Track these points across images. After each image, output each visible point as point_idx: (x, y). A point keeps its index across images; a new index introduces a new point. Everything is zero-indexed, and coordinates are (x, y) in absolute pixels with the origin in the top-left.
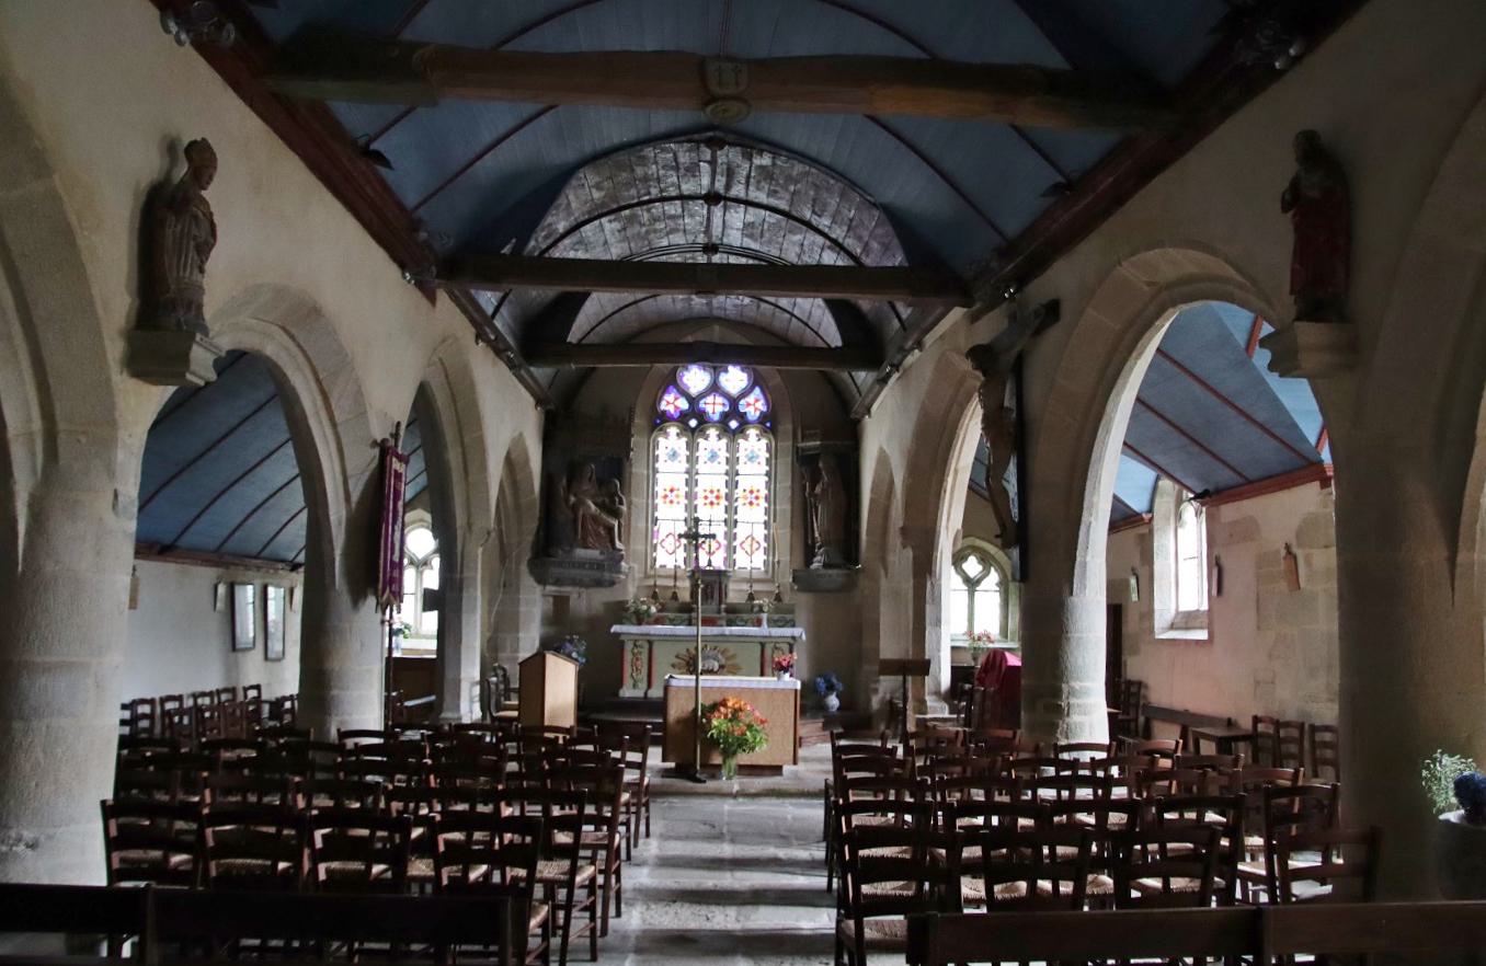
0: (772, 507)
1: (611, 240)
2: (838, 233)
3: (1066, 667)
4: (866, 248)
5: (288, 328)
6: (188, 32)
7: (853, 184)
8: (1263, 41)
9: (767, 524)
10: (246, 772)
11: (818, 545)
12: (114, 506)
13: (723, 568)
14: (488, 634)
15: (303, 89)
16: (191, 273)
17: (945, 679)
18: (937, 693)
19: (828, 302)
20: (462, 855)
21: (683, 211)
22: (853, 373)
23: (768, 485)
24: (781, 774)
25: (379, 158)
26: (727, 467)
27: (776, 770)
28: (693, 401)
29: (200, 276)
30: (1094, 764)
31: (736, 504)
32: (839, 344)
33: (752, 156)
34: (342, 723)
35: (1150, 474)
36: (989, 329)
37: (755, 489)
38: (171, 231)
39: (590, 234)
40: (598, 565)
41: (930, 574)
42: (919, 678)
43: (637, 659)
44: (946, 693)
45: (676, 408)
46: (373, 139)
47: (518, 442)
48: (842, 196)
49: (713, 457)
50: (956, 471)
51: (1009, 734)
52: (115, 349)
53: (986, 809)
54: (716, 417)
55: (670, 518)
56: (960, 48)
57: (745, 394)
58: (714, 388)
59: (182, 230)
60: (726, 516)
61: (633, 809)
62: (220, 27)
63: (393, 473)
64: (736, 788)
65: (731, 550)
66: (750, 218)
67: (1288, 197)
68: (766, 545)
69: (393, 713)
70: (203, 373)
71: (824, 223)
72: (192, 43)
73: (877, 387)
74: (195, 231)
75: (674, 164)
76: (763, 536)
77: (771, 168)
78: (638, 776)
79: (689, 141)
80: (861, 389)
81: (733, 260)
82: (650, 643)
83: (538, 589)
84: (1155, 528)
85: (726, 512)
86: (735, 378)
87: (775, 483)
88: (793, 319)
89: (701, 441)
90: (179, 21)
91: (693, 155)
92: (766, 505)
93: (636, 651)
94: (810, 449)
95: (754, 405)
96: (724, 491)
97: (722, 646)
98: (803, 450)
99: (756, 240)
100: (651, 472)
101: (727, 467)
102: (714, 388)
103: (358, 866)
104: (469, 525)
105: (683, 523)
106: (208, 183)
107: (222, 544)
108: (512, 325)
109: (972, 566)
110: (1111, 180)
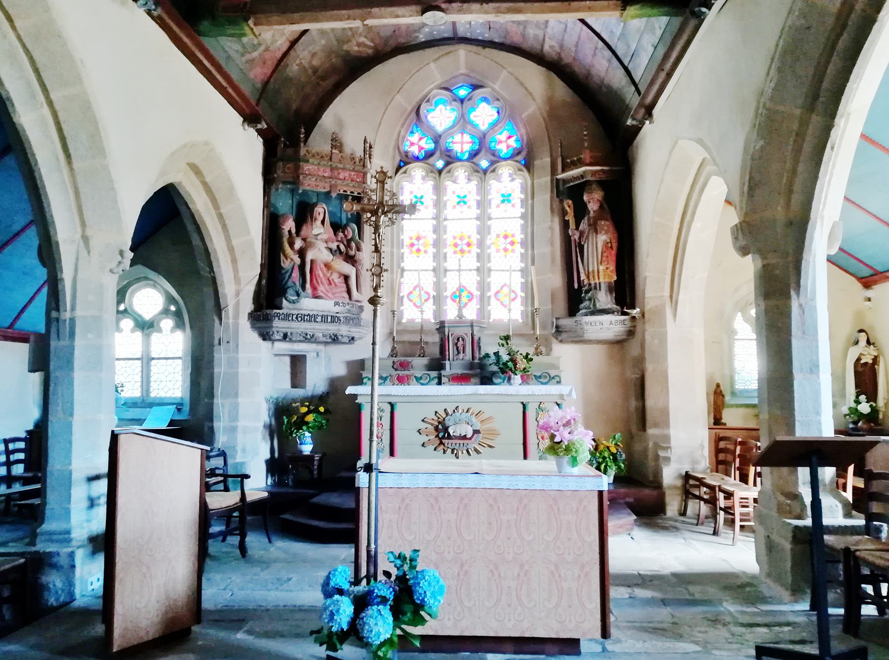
0: (530, 252)
9: (524, 272)
11: (584, 289)
14: (805, 512)
23: (524, 228)
28: (437, 139)
31: (489, 251)
37: (509, 233)
45: (421, 148)
49: (462, 201)
54: (466, 156)
60: (479, 265)
65: (484, 300)
68: (523, 295)
69: (24, 495)
76: (519, 286)
82: (392, 406)
85: (478, 261)
87: (533, 225)
89: (449, 184)
92: (523, 251)
97: (475, 408)
98: (565, 181)
105: (432, 273)
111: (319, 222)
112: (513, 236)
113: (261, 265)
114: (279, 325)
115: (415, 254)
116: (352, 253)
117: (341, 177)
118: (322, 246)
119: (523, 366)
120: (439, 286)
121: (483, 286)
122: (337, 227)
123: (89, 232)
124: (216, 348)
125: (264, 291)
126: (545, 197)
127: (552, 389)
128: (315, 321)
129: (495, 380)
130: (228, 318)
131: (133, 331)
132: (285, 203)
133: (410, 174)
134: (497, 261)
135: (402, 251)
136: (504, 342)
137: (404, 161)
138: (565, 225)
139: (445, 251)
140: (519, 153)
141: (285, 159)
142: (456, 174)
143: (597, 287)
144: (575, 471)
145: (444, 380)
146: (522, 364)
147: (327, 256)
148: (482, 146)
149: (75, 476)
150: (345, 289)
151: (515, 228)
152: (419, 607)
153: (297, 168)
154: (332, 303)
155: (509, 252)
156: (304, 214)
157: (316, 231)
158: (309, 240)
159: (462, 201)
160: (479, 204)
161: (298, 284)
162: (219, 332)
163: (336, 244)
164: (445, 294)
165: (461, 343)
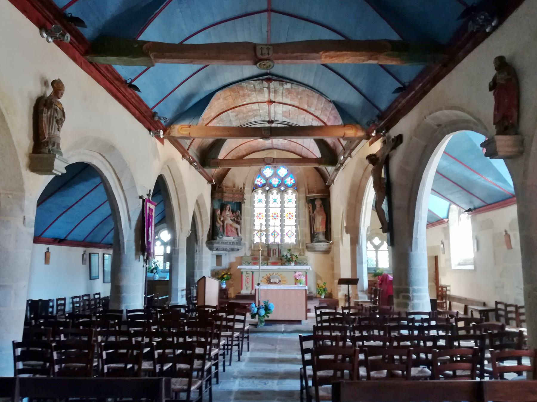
0: (298, 219)
1: (232, 119)
2: (317, 113)
3: (411, 281)
4: (329, 119)
5: (101, 153)
6: (51, 37)
7: (321, 94)
8: (480, 21)
9: (296, 226)
10: (81, 327)
12: (24, 222)
13: (280, 243)
15: (101, 60)
16: (54, 131)
17: (366, 285)
18: (362, 291)
19: (315, 140)
20: (163, 359)
21: (259, 108)
22: (327, 168)
24: (301, 324)
25: (136, 88)
26: (281, 205)
27: (299, 322)
28: (267, 179)
29: (58, 132)
30: (423, 320)
31: (284, 219)
32: (320, 156)
33: (283, 85)
34: (127, 306)
35: (447, 203)
36: (376, 147)
38: (46, 115)
39: (224, 117)
40: (233, 243)
41: (358, 244)
42: (355, 286)
43: (248, 279)
44: (366, 291)
46: (133, 81)
47: (201, 196)
48: (318, 99)
49: (275, 201)
50: (366, 203)
51: (388, 307)
52: (23, 161)
53: (375, 338)
54: (276, 186)
55: (259, 223)
56: (358, 35)
57: (286, 176)
58: (275, 175)
59: (50, 115)
60: (281, 223)
61: (241, 339)
62: (63, 35)
63: (148, 208)
64: (283, 330)
65: (282, 236)
66: (284, 110)
67: (491, 84)
68: (296, 234)
70: (60, 170)
71: (312, 110)
72: (54, 41)
73: (335, 173)
74: (56, 115)
75: (254, 89)
77: (291, 89)
78: (243, 326)
79: (259, 80)
80: (330, 174)
81: (279, 125)
82: (253, 272)
83: (210, 252)
84: (450, 225)
86: (283, 171)
87: (299, 210)
88: (304, 148)
90: (48, 33)
91: (261, 85)
92: (296, 219)
93: (247, 275)
94: (311, 197)
95: (290, 181)
96: (279, 214)
97: (280, 273)
98: (309, 197)
99: (287, 118)
100: (252, 207)
101: (281, 205)
102: (275, 175)
103: (122, 365)
104: (181, 229)
106: (61, 96)
107: (102, 240)
108: (196, 152)
109: (377, 241)
110: (421, 84)
111: (228, 211)
112: (292, 213)
113: (210, 226)
114: (216, 245)
115: (259, 219)
116: (239, 221)
117: (236, 196)
118: (229, 219)
119: (295, 260)
121: (282, 231)
122: (233, 212)
123: (182, 227)
124: (195, 253)
125: (211, 234)
126: (303, 201)
127: (304, 267)
128: (227, 244)
129: (286, 264)
130: (199, 243)
131: (160, 245)
132: (217, 206)
133: (257, 192)
134: (287, 222)
135: (254, 218)
136: (288, 251)
137: (255, 188)
138: (310, 212)
139: (269, 218)
140: (294, 186)
141: (219, 192)
142: (273, 192)
143: (319, 233)
144: (301, 285)
145: (269, 264)
146: (294, 258)
147: (231, 222)
148: (282, 183)
149: (179, 290)
150: (236, 233)
151: (293, 211)
152: (270, 310)
153: (223, 195)
154: (232, 238)
155: (291, 219)
156: (223, 208)
157: (227, 214)
158: (225, 217)
159: (275, 201)
160: (281, 202)
161: (222, 232)
162: (197, 248)
163: (233, 218)
164: (269, 233)
165: (275, 251)
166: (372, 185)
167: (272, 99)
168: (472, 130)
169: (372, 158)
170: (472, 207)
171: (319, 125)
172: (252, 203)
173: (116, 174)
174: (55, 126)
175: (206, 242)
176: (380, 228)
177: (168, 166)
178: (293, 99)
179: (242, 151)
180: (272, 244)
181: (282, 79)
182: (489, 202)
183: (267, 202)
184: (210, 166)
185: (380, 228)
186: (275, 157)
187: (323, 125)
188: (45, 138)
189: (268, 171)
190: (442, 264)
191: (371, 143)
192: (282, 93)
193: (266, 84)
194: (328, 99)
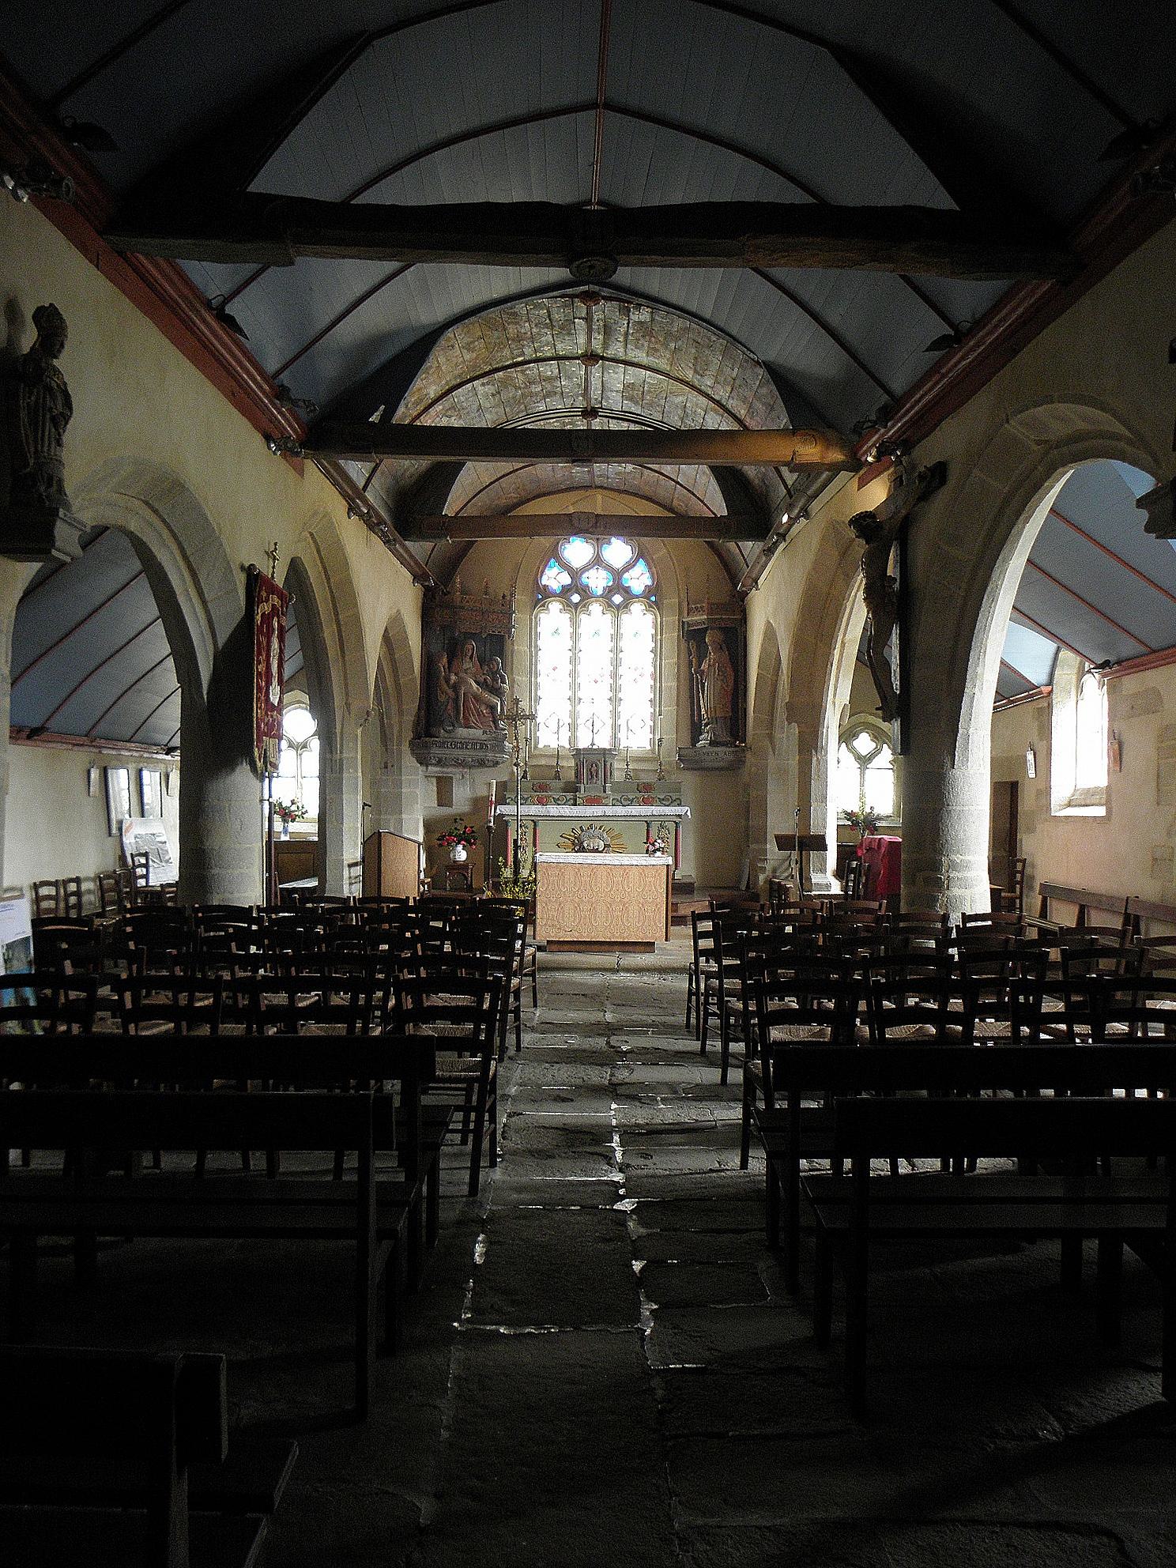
2: (721, 394)
19: (713, 469)
28: (575, 574)
35: (1050, 646)
36: (876, 494)
47: (396, 620)
54: (600, 592)
58: (597, 561)
59: (36, 402)
75: (548, 321)
81: (614, 426)
83: (422, 769)
86: (618, 551)
89: (583, 617)
97: (607, 825)
99: (636, 403)
109: (864, 743)
120: (574, 715)
126: (672, 636)
148: (617, 586)
156: (454, 651)
157: (465, 667)
166: (861, 595)
167: (597, 345)
168: (1122, 457)
169: (865, 524)
170: (1112, 659)
171: (724, 427)
172: (533, 636)
173: (185, 557)
174: (50, 430)
175: (411, 743)
176: (877, 709)
177: (311, 534)
178: (656, 350)
179: (509, 490)
180: (589, 751)
181: (624, 296)
182: (1154, 645)
183: (575, 637)
184: (422, 536)
185: (877, 709)
186: (599, 512)
187: (736, 427)
188: (27, 465)
189: (577, 551)
190: (1027, 801)
191: (862, 484)
192: (627, 334)
193: (581, 308)
194: (752, 355)
